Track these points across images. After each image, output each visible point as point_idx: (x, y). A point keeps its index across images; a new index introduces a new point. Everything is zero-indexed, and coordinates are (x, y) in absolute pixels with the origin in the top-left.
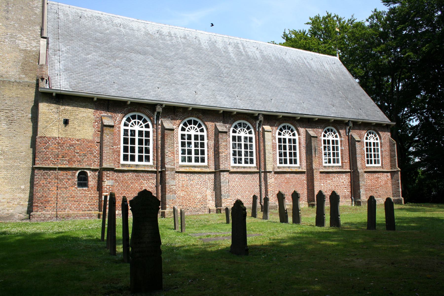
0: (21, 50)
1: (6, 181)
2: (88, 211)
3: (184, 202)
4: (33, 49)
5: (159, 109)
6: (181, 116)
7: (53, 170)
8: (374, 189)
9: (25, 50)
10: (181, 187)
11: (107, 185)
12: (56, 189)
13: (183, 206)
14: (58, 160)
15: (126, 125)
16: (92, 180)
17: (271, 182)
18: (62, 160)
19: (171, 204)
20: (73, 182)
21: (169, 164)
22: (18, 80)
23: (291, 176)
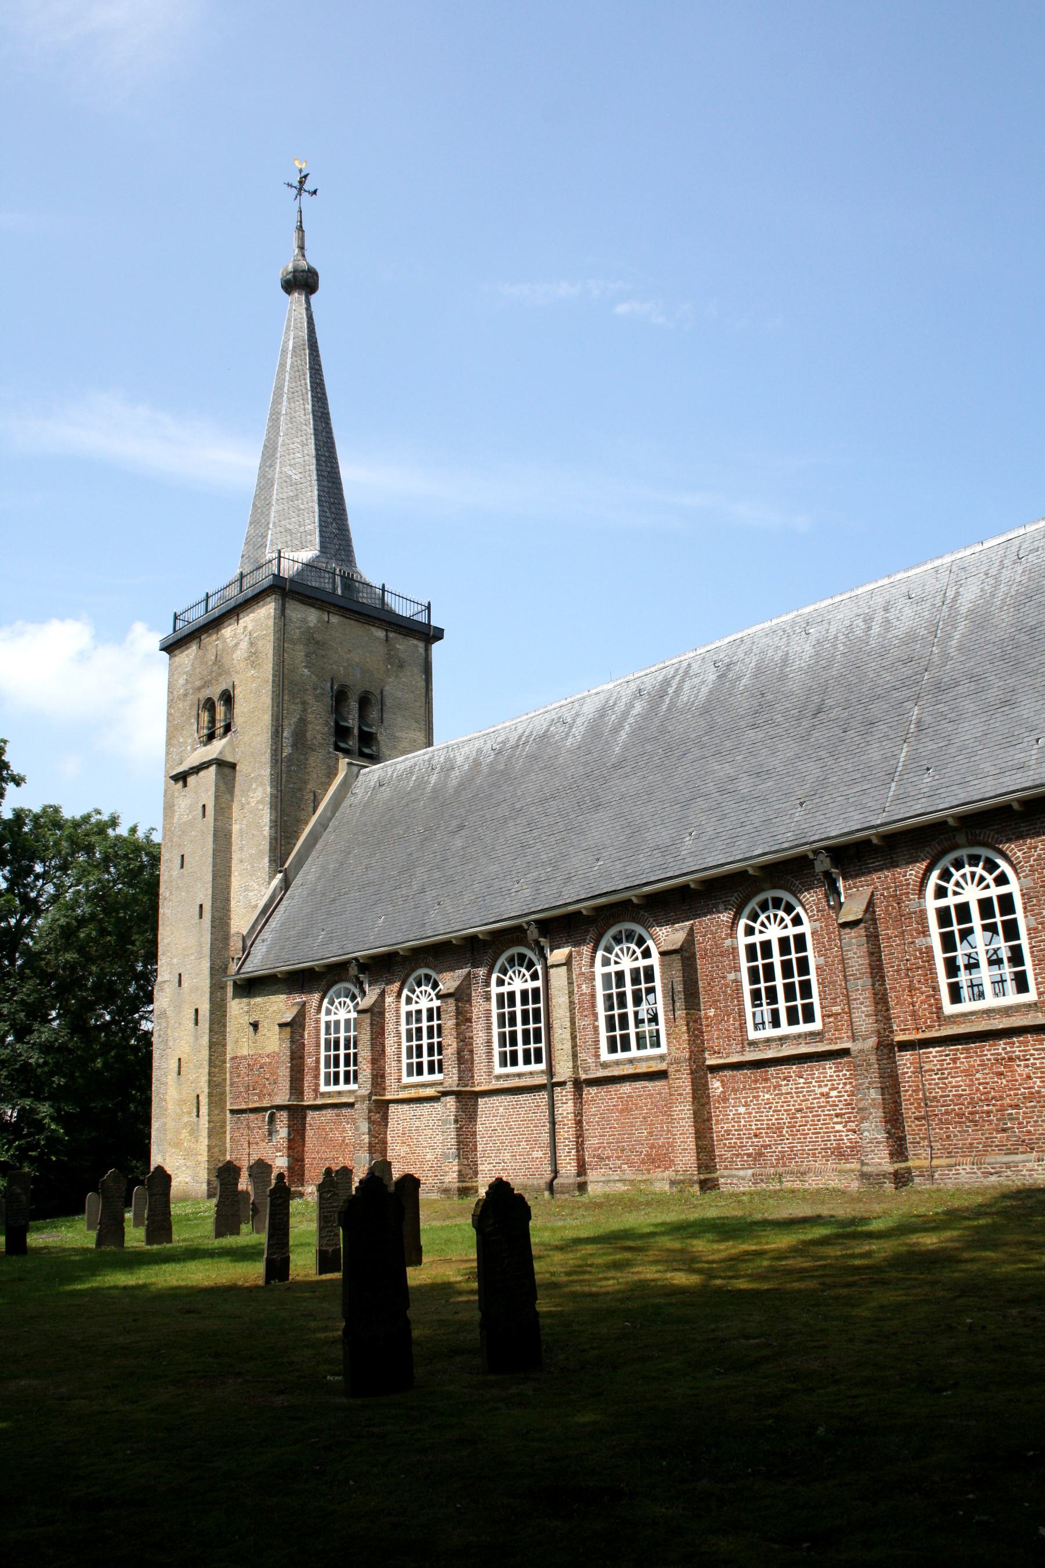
8: (988, 1113)
15: (941, 893)
17: (565, 1113)
23: (636, 1088)
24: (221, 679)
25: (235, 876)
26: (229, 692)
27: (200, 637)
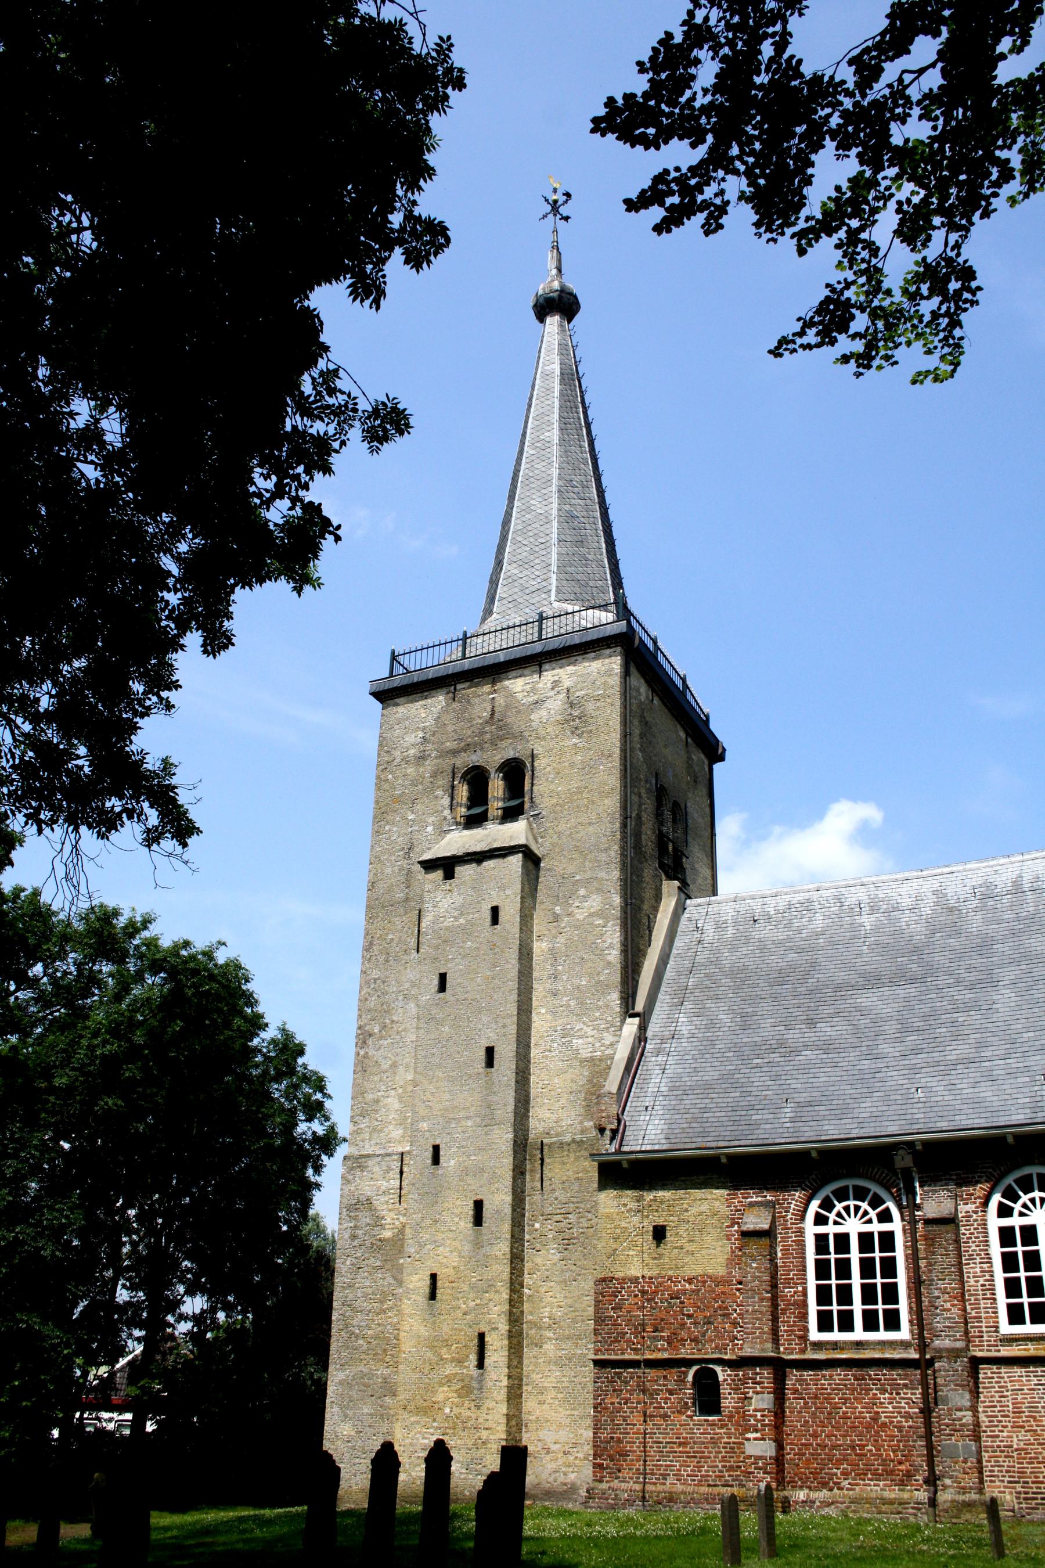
0: (582, 1061)
1: (560, 1396)
2: (723, 1486)
3: (1028, 1471)
4: (607, 1053)
5: (903, 1160)
6: (988, 1168)
7: (634, 1368)
9: (591, 1060)
10: (1011, 1415)
11: (755, 1410)
12: (642, 1419)
13: (1024, 1482)
14: (643, 1337)
15: (820, 1220)
16: (730, 1394)
18: (654, 1338)
19: (960, 1476)
20: (682, 1399)
21: (946, 1336)
22: (578, 1137)
24: (505, 744)
25: (538, 1014)
26: (523, 763)
27: (455, 685)
